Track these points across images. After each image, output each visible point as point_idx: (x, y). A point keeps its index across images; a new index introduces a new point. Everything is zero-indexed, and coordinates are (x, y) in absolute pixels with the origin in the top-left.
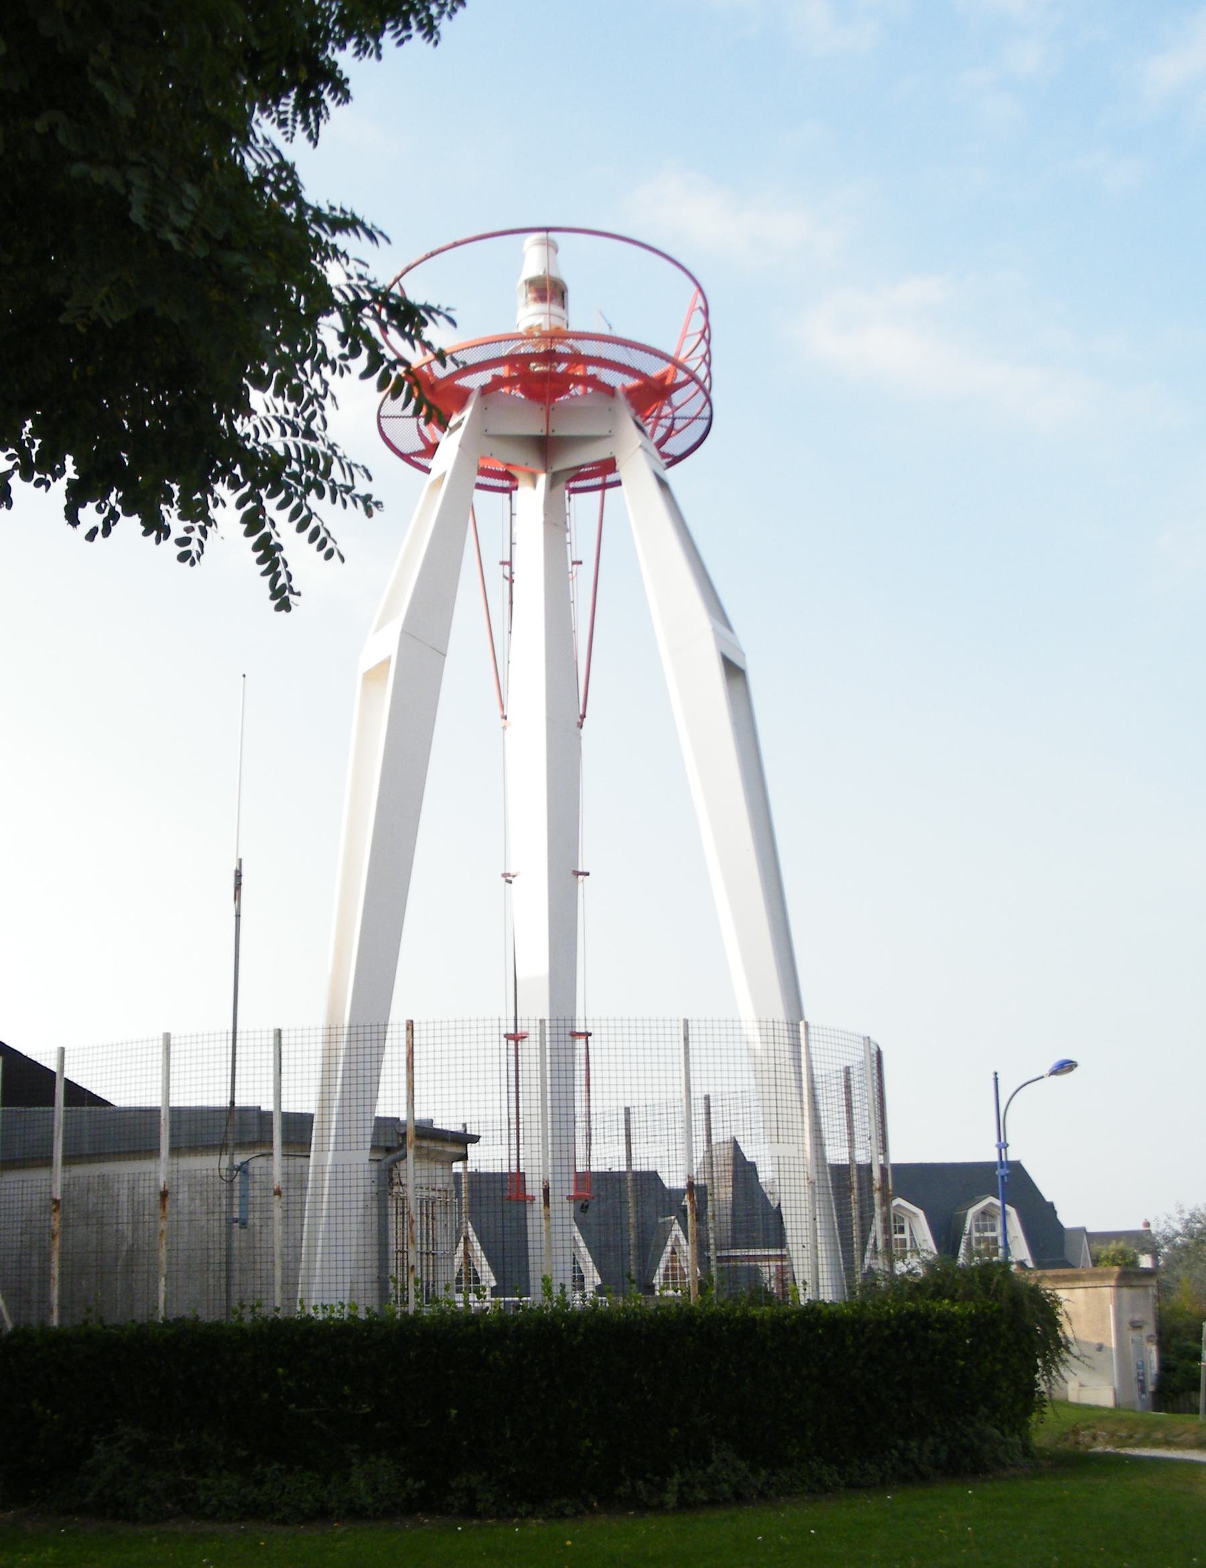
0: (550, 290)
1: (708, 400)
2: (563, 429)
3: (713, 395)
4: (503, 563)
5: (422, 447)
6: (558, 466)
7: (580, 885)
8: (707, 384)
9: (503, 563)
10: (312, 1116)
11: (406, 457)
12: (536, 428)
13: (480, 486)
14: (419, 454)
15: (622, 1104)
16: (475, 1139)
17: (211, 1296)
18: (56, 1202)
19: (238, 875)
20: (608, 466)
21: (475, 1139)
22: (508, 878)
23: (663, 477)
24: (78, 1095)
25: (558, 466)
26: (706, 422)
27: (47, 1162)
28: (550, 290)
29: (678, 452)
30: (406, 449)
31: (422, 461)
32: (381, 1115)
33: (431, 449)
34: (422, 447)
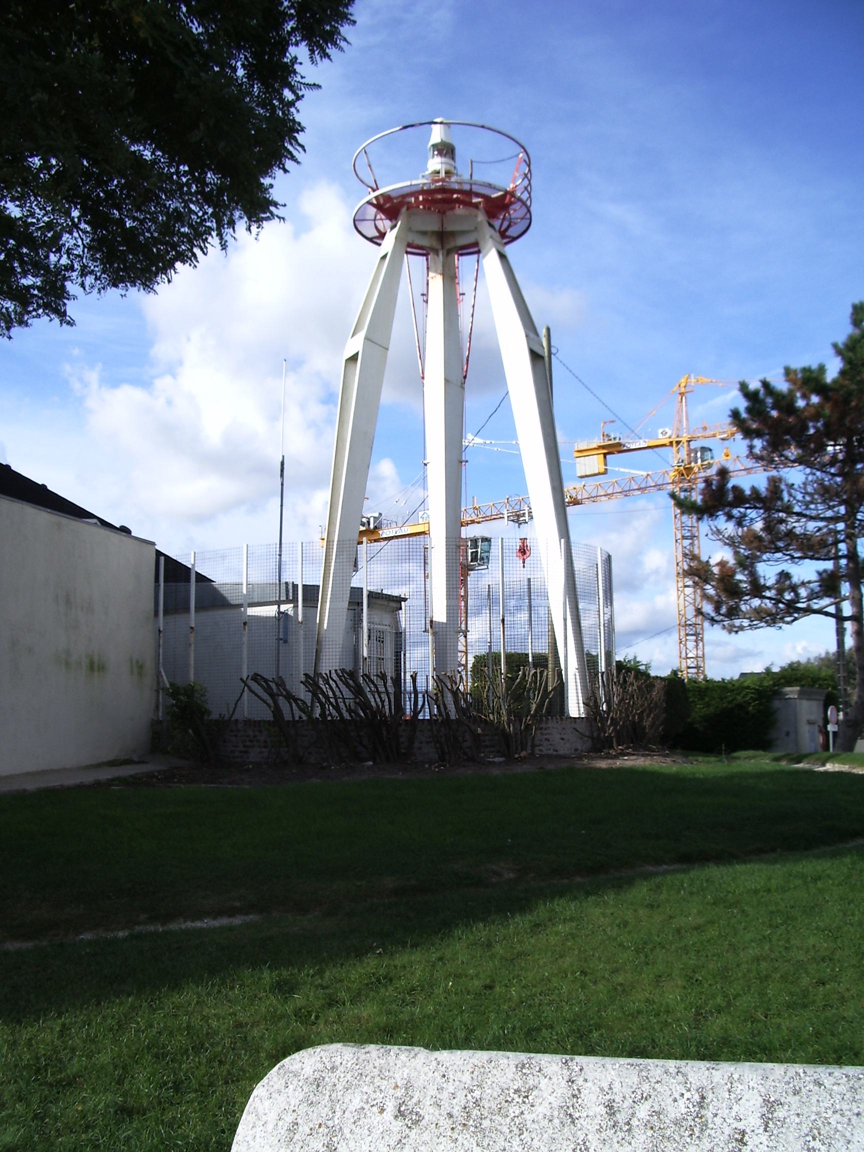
0: (446, 150)
1: (529, 211)
2: (450, 228)
3: (532, 209)
4: (423, 295)
5: (377, 234)
6: (448, 247)
7: (463, 468)
8: (528, 203)
9: (423, 295)
10: (319, 586)
11: (371, 240)
12: (435, 227)
13: (407, 253)
14: (375, 238)
15: (487, 583)
16: (405, 600)
17: (768, 604)
18: (192, 628)
19: (282, 464)
20: (476, 244)
21: (405, 600)
22: (425, 465)
23: (502, 251)
24: (201, 578)
25: (448, 247)
26: (528, 221)
27: (187, 609)
28: (446, 150)
29: (515, 235)
30: (370, 235)
31: (378, 241)
32: (355, 586)
33: (382, 235)
34: (377, 234)
